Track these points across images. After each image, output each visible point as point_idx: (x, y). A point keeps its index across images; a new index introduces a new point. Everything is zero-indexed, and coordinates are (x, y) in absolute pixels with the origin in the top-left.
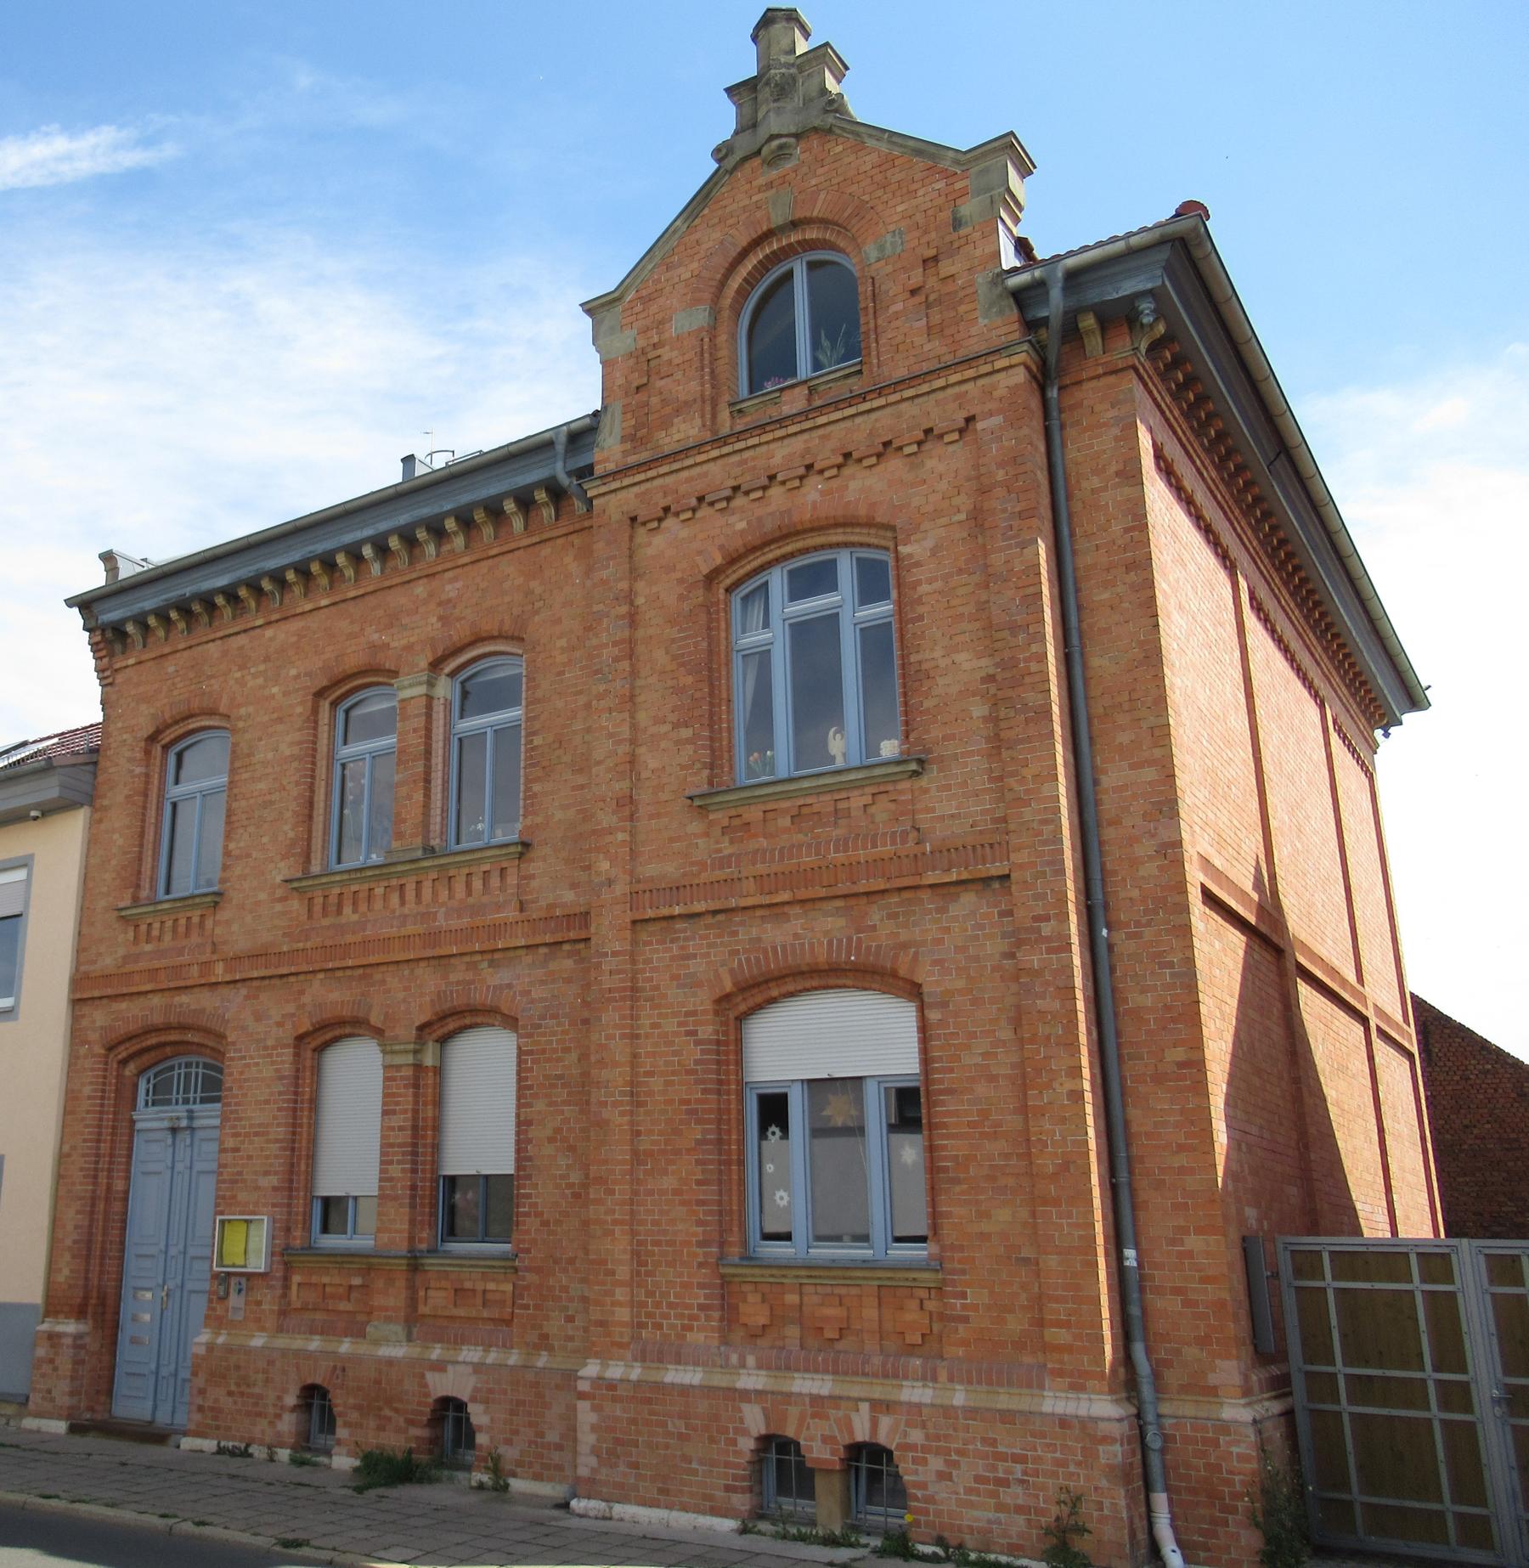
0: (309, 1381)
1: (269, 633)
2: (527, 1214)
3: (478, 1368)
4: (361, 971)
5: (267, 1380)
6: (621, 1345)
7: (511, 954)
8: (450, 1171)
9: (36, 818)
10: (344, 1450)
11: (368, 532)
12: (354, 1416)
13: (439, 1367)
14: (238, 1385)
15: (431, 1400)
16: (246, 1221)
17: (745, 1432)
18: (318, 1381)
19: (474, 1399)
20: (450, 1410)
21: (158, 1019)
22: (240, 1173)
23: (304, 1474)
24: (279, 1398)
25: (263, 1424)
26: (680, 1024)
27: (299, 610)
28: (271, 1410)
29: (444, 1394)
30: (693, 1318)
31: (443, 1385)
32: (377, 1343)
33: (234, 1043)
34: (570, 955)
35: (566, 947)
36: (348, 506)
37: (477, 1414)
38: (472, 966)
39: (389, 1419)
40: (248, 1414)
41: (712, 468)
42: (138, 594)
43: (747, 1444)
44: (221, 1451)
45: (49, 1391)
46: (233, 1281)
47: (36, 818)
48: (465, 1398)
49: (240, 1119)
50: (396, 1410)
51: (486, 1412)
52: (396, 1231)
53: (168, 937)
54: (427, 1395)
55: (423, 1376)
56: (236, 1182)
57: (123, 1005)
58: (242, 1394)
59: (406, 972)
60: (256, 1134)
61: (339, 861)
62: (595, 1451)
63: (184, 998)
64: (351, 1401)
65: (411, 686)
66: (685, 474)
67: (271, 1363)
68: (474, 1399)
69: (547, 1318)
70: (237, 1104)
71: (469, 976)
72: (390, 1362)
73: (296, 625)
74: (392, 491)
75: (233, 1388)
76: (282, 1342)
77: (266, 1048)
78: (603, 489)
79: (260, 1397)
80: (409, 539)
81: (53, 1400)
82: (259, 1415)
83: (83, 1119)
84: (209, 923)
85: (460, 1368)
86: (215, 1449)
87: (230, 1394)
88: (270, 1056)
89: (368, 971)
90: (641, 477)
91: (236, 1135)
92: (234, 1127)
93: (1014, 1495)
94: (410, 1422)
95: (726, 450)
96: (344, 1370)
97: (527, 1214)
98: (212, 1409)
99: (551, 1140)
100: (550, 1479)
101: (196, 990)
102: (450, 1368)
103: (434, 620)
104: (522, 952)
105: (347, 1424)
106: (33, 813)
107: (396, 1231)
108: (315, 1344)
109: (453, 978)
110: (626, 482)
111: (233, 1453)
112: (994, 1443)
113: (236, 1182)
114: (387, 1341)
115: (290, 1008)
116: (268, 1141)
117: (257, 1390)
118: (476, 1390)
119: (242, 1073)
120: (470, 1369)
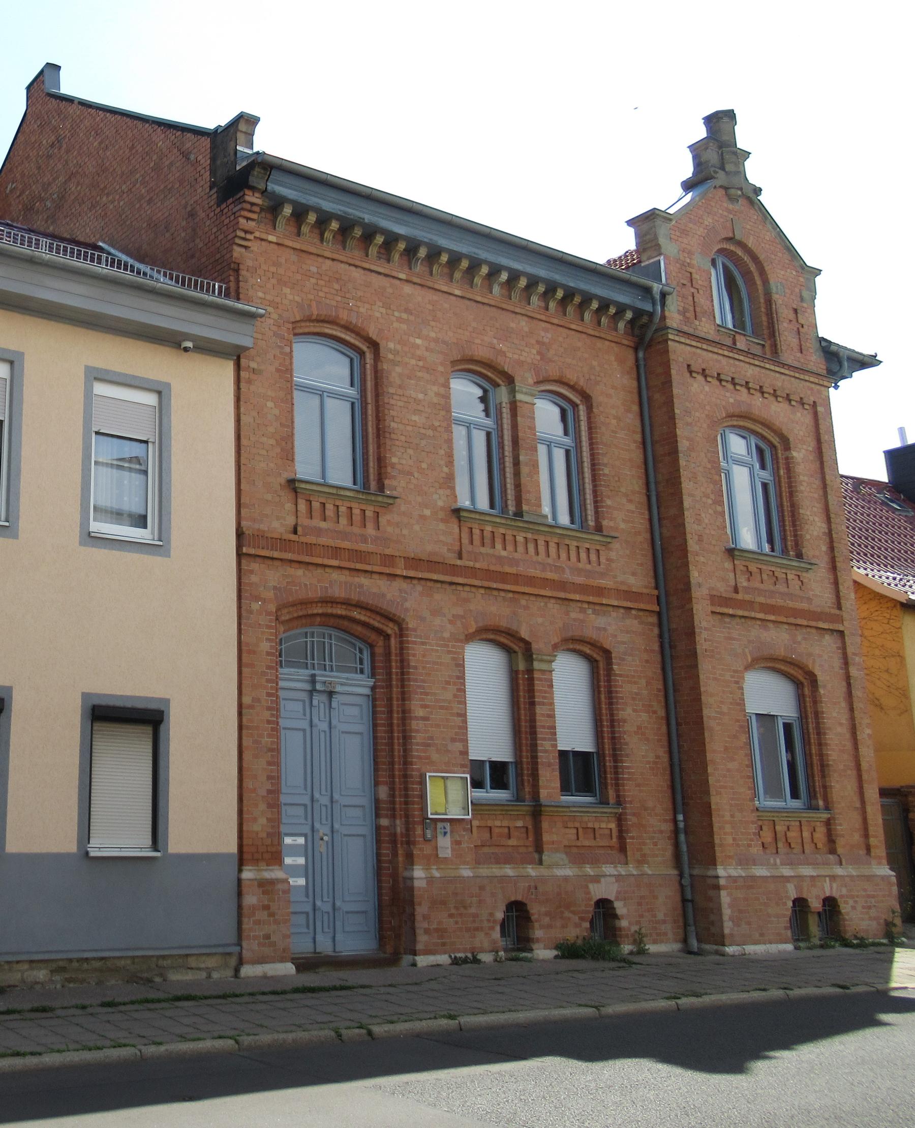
0: (513, 899)
1: (408, 289)
2: (629, 779)
3: (619, 878)
4: (511, 595)
5: (480, 902)
6: (730, 857)
7: (604, 608)
8: (561, 747)
9: (186, 350)
10: (542, 945)
11: (491, 258)
12: (547, 920)
13: (596, 879)
14: (457, 908)
15: (593, 903)
16: (443, 777)
17: (788, 897)
18: (519, 898)
19: (617, 899)
20: (604, 907)
21: (338, 592)
22: (431, 738)
23: (515, 967)
24: (491, 914)
25: (481, 936)
26: (732, 677)
27: (436, 286)
28: (486, 924)
29: (598, 897)
30: (752, 840)
31: (599, 891)
32: (550, 867)
33: (415, 630)
34: (636, 617)
35: (634, 612)
36: (530, 245)
37: (620, 908)
38: (582, 611)
39: (569, 918)
40: (468, 930)
41: (724, 361)
42: (383, 210)
43: (790, 904)
44: (456, 962)
45: (267, 937)
46: (440, 825)
47: (186, 350)
48: (612, 899)
49: (427, 694)
50: (574, 913)
51: (625, 905)
52: (553, 788)
53: (343, 521)
54: (590, 899)
55: (587, 887)
56: (429, 745)
57: (300, 572)
58: (461, 915)
59: (542, 604)
60: (442, 708)
61: (97, 433)
62: (731, 919)
63: (364, 580)
64: (543, 910)
65: (526, 394)
66: (716, 356)
67: (482, 888)
68: (617, 899)
69: (644, 844)
70: (423, 681)
71: (581, 616)
72: (566, 879)
73: (430, 296)
74: (524, 243)
75: (453, 911)
76: (484, 871)
77: (443, 639)
78: (677, 338)
79: (476, 916)
80: (300, 214)
81: (273, 944)
82: (477, 929)
83: (264, 674)
84: (383, 520)
85: (608, 879)
86: (449, 961)
87: (451, 916)
88: (447, 646)
89: (516, 596)
90: (694, 343)
91: (426, 706)
92: (422, 700)
93: (873, 912)
94: (582, 919)
95: (731, 354)
96: (536, 888)
97: (629, 779)
98: (437, 930)
99: (636, 733)
100: (662, 942)
101: (375, 576)
102: (603, 880)
103: (535, 352)
104: (611, 609)
105: (541, 927)
106: (189, 344)
107: (553, 788)
108: (509, 871)
109: (573, 615)
110: (688, 341)
111: (465, 961)
112: (865, 890)
113: (429, 745)
114: (557, 865)
115: (459, 611)
116: (452, 714)
117: (473, 910)
118: (618, 892)
119: (424, 656)
120: (613, 879)
